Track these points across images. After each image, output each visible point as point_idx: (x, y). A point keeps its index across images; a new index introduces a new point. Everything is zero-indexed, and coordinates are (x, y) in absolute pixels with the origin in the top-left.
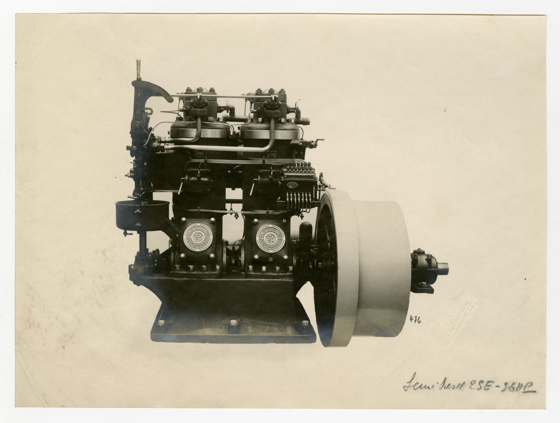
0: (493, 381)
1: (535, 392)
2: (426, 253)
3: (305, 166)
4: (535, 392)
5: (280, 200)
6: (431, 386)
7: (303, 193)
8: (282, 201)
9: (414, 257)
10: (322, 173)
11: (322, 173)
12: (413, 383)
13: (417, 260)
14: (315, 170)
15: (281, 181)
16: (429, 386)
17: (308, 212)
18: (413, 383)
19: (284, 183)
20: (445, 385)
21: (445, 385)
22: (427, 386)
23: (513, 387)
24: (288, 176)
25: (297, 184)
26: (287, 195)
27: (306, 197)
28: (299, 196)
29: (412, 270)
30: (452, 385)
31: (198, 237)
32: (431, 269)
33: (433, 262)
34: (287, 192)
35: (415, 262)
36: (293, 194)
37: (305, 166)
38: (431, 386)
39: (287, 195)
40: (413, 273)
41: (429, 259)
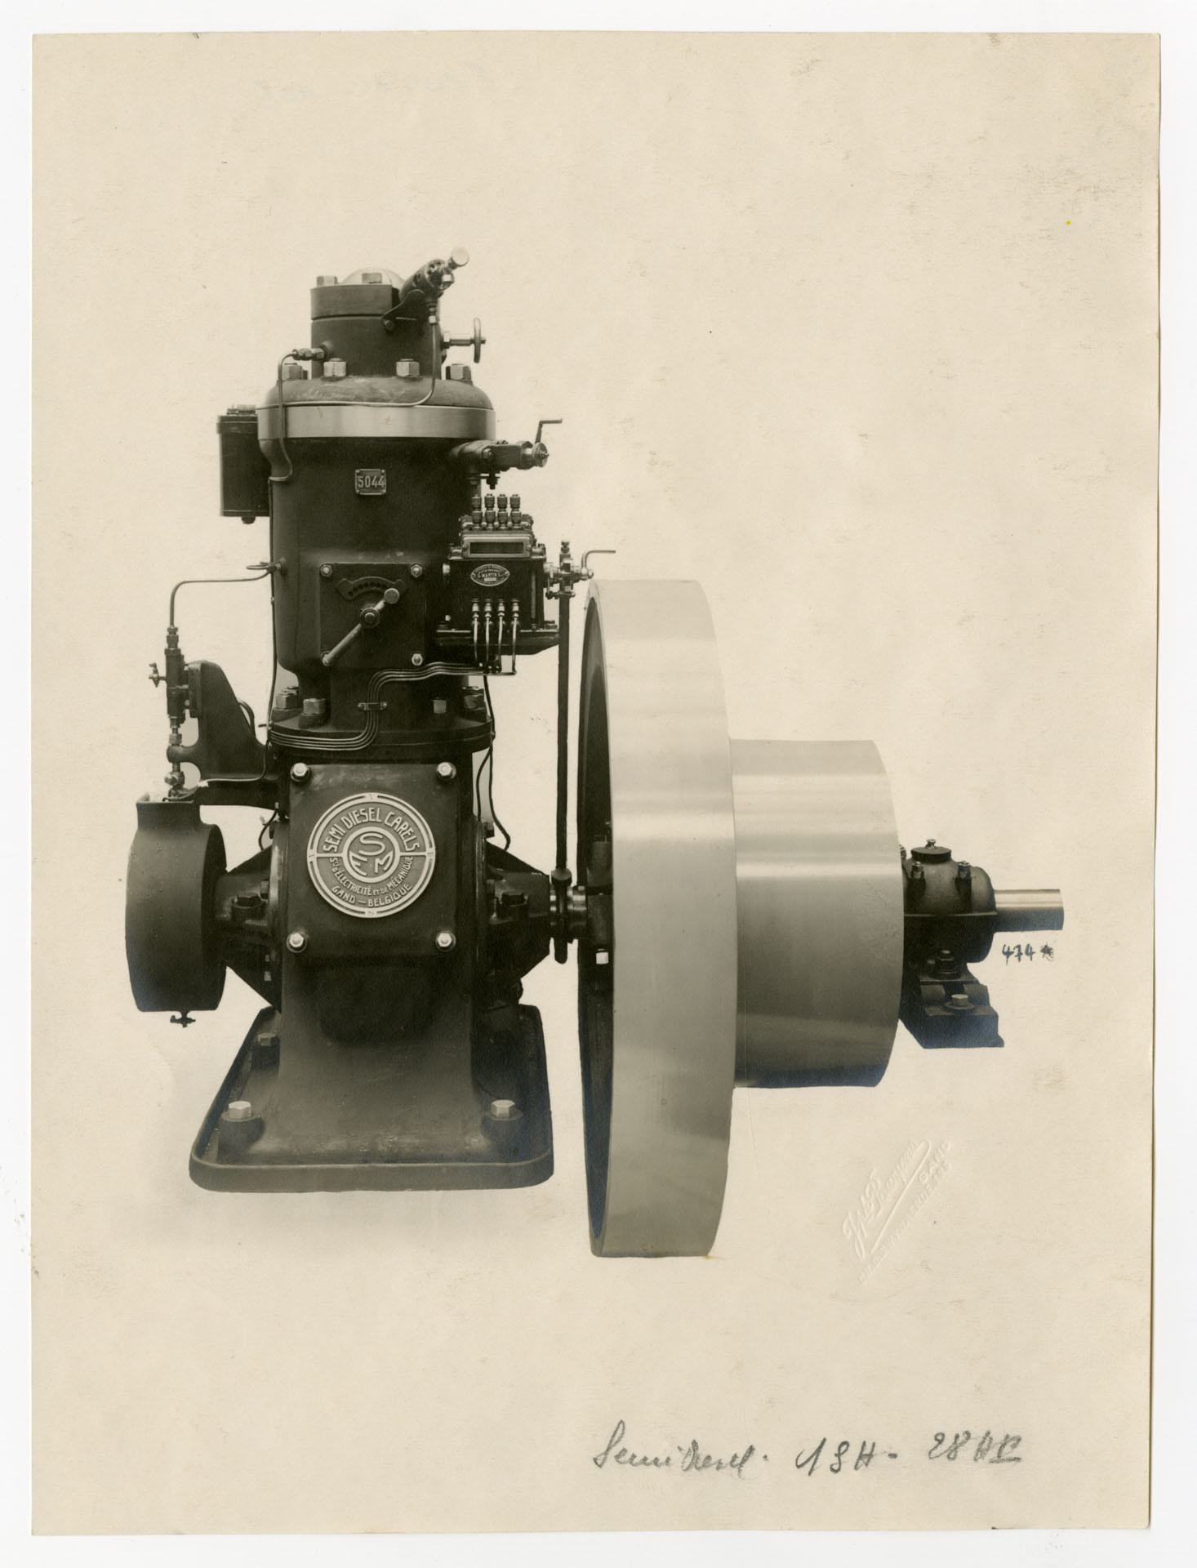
0: (822, 1439)
1: (1019, 1459)
2: (956, 857)
3: (502, 506)
4: (1019, 1459)
5: (450, 625)
6: (662, 1459)
7: (515, 600)
8: (453, 631)
9: (912, 873)
10: (568, 544)
11: (568, 544)
12: (615, 1451)
13: (922, 881)
14: (532, 522)
15: (452, 563)
16: (656, 1459)
17: (511, 671)
18: (615, 1451)
19: (465, 566)
20: (697, 1459)
21: (697, 1459)
22: (651, 1459)
23: (945, 1446)
24: (476, 547)
25: (507, 572)
26: (475, 608)
27: (488, 615)
28: (476, 615)
29: (906, 919)
30: (714, 1460)
31: (444, 768)
32: (970, 911)
33: (977, 885)
34: (489, 600)
35: (914, 888)
36: (495, 607)
37: (502, 506)
38: (662, 1459)
39: (475, 608)
40: (909, 925)
41: (964, 877)
